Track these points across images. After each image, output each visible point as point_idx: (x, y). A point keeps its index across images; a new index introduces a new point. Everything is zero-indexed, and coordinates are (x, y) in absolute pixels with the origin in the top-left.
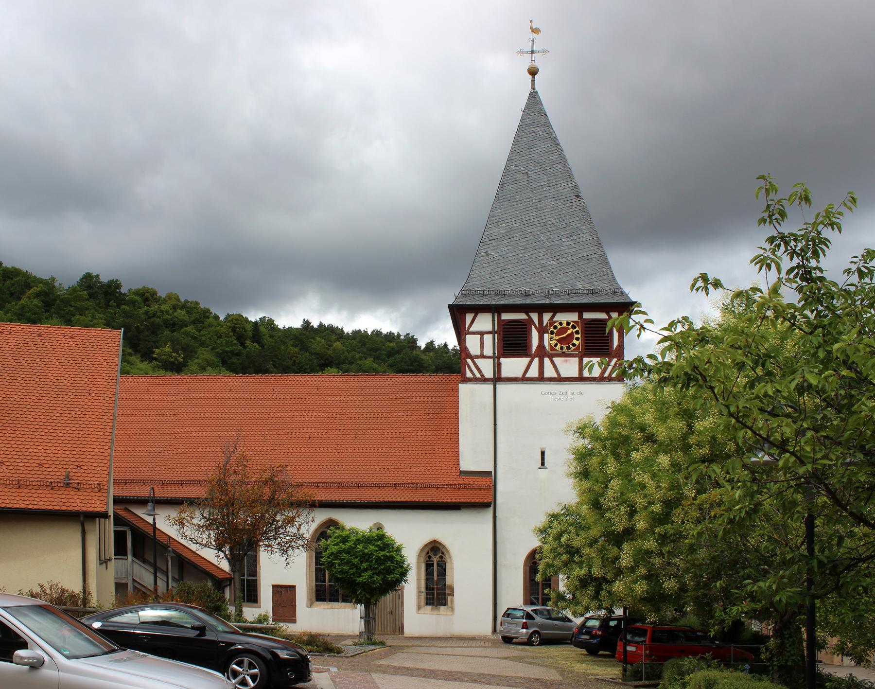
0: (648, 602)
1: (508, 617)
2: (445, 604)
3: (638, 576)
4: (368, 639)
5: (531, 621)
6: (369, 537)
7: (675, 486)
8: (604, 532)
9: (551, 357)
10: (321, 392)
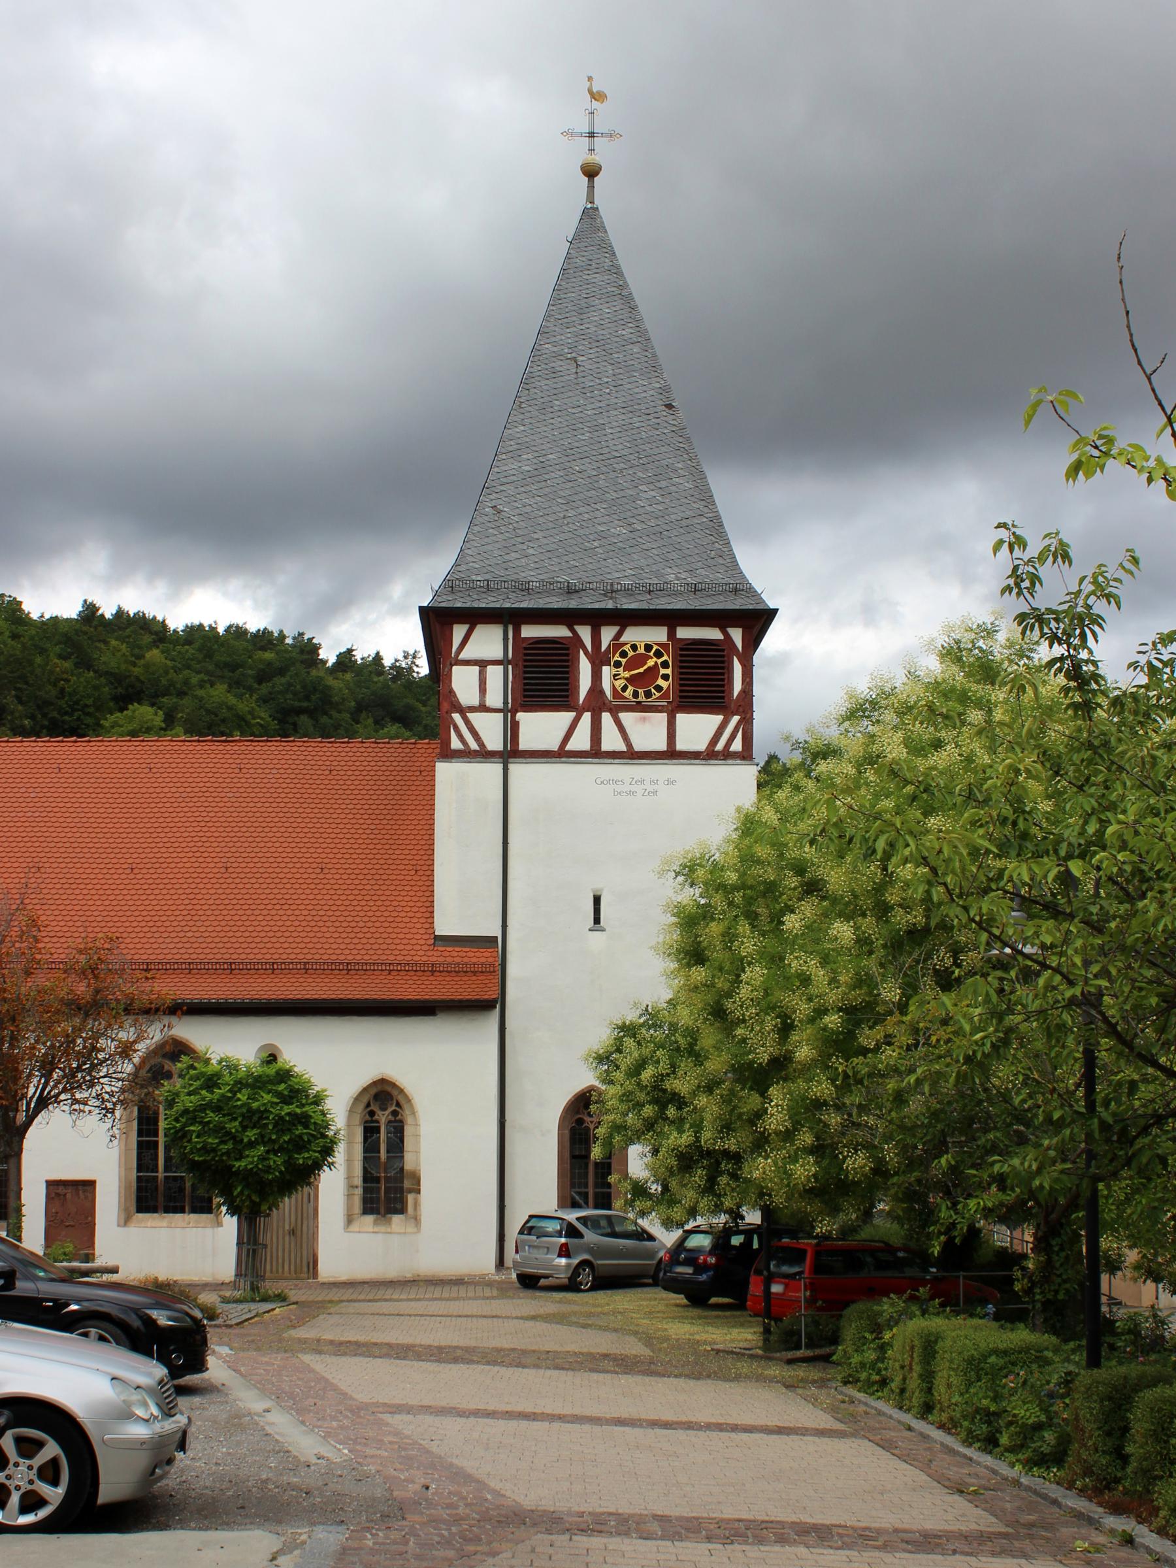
0: (816, 1196)
1: (529, 1234)
2: (402, 1210)
3: (798, 1148)
4: (252, 1289)
5: (576, 1240)
6: (260, 1076)
7: (863, 981)
8: (733, 1065)
9: (614, 711)
10: (158, 775)
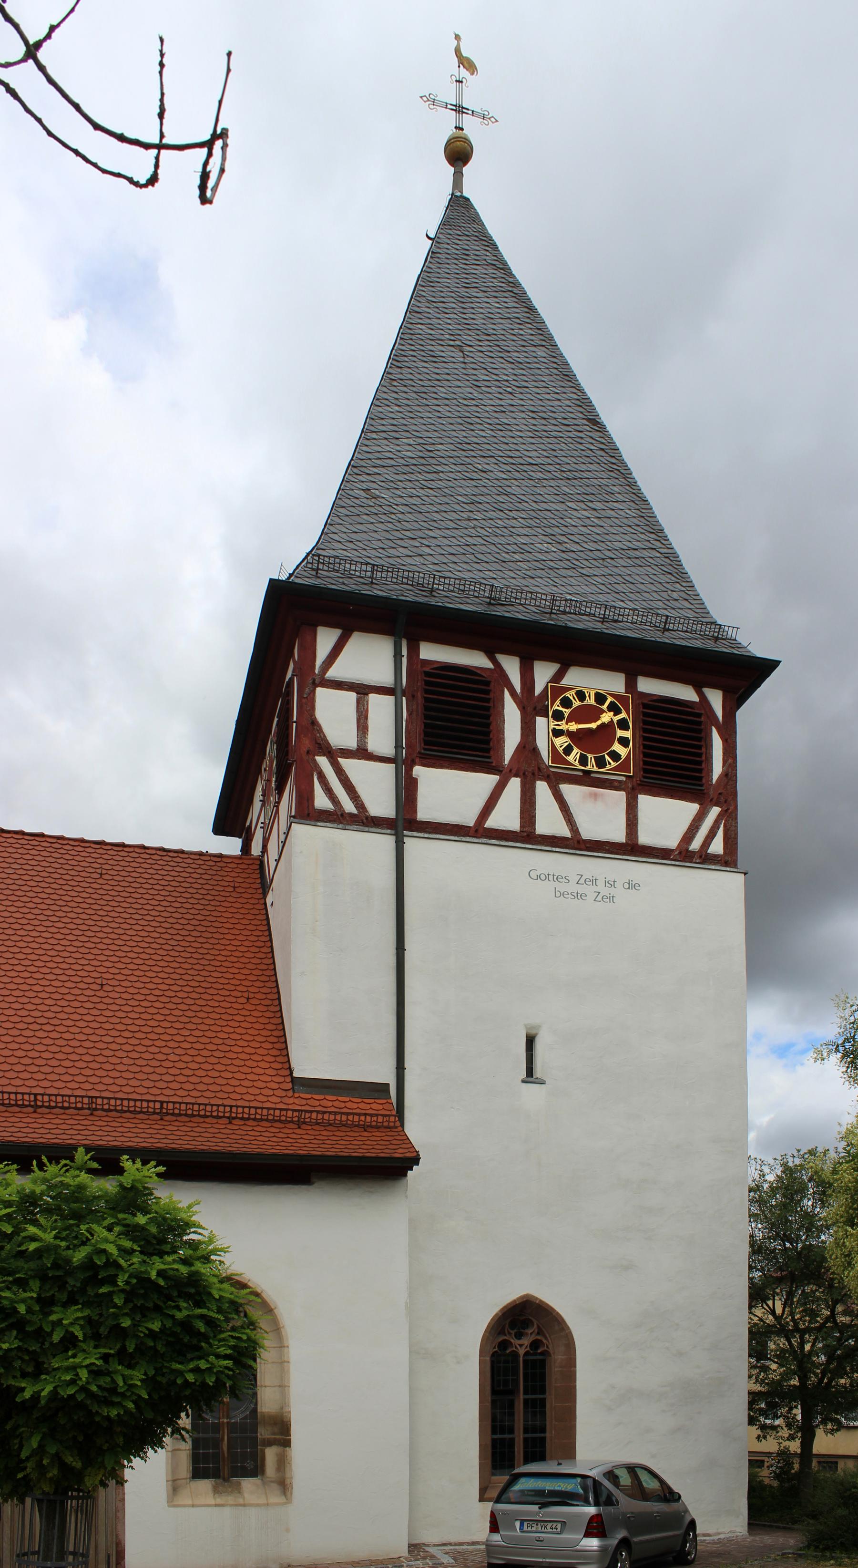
2: (256, 1470)
9: (554, 781)
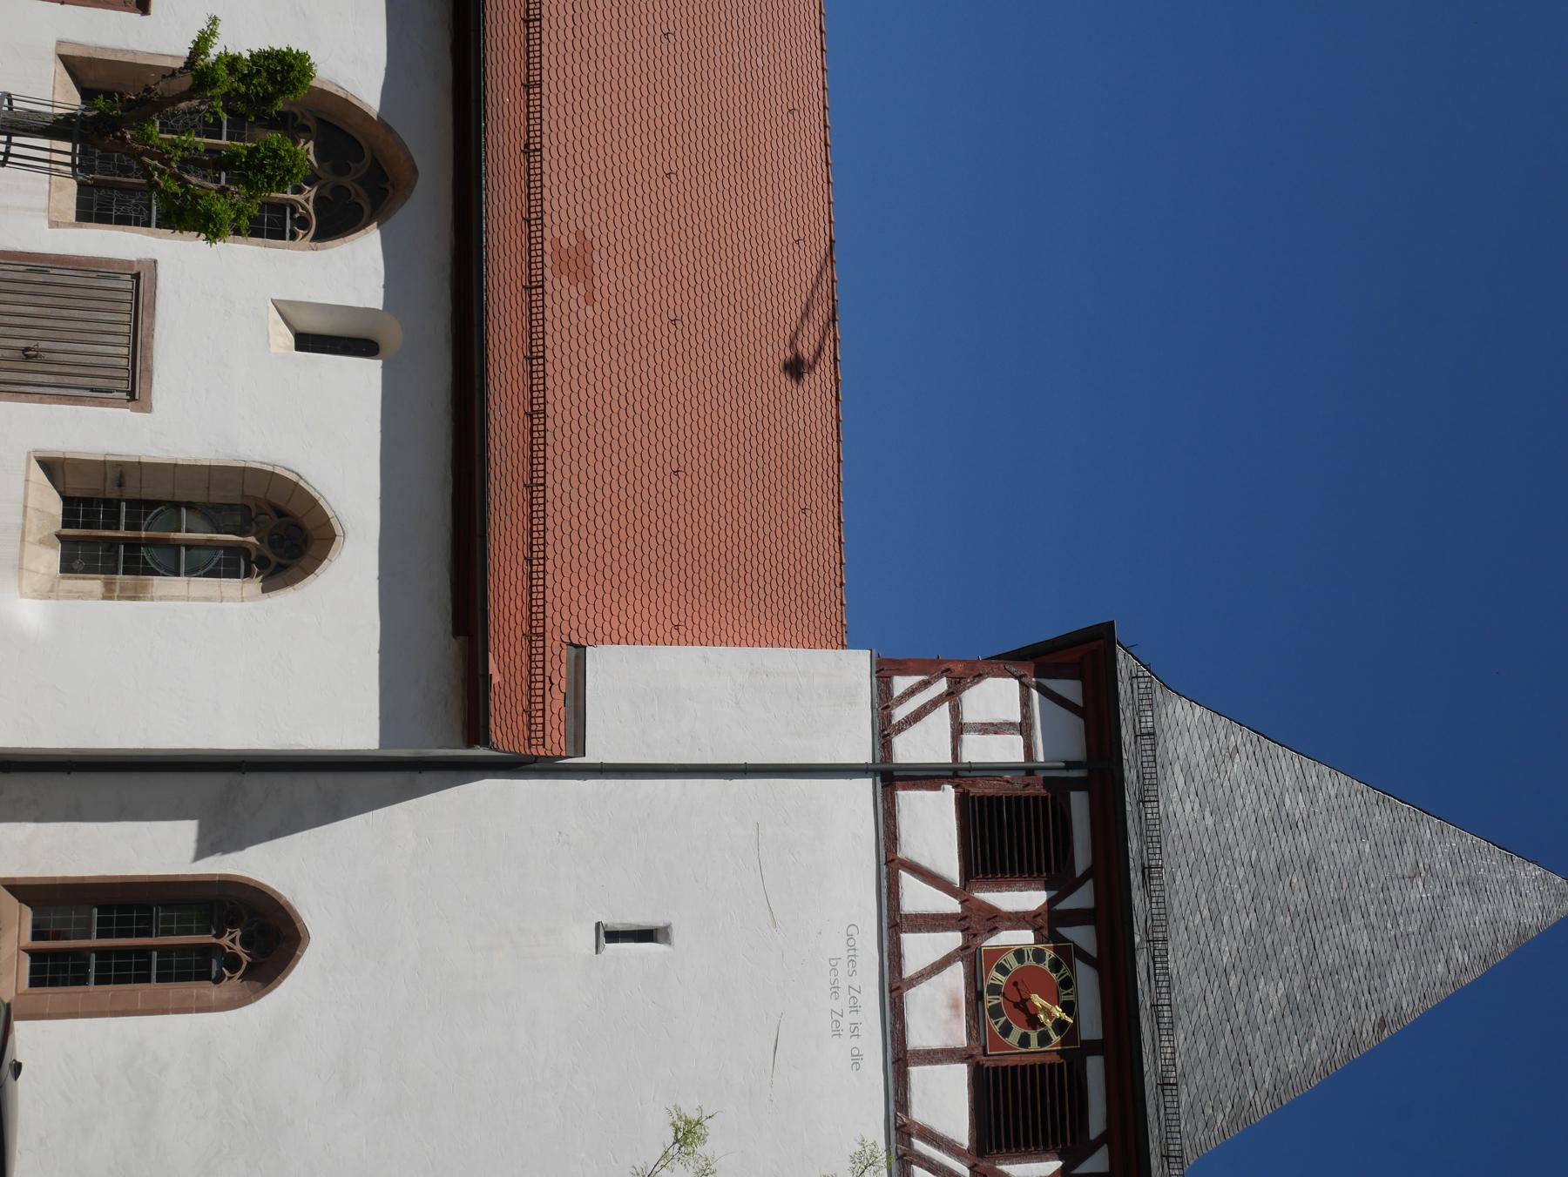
2: (67, 567)
